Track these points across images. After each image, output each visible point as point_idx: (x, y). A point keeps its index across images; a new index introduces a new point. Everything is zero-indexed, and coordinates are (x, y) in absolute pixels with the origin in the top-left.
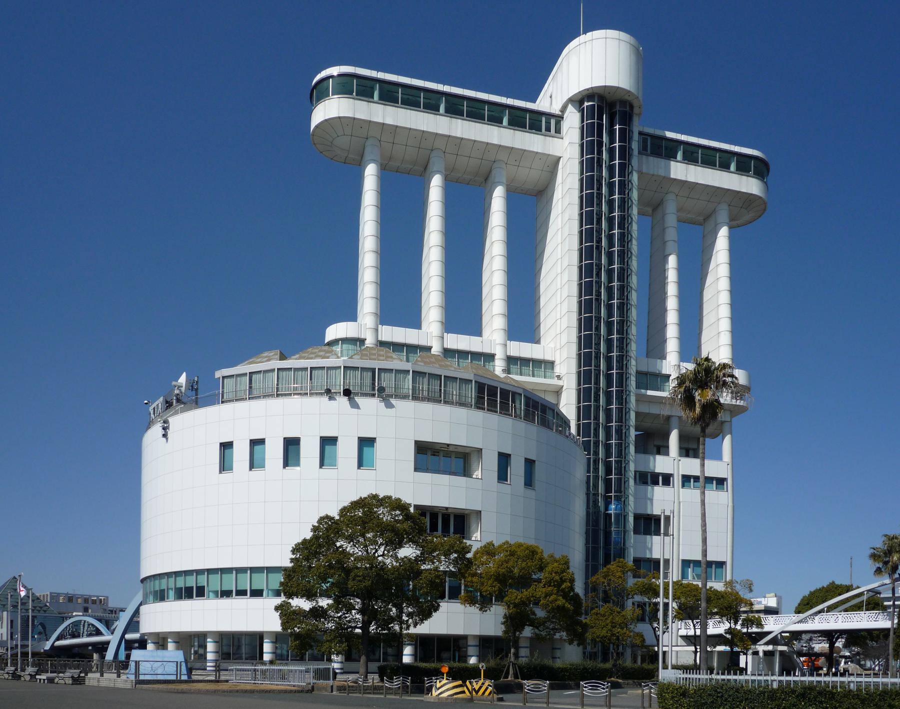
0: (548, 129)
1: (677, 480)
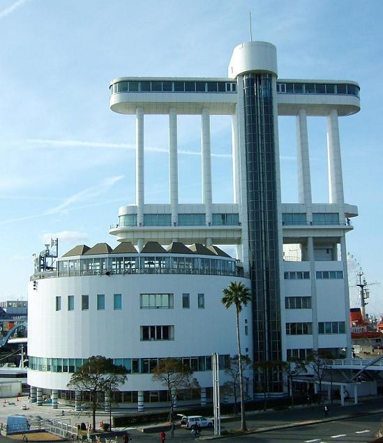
0: (229, 89)
1: (315, 328)
